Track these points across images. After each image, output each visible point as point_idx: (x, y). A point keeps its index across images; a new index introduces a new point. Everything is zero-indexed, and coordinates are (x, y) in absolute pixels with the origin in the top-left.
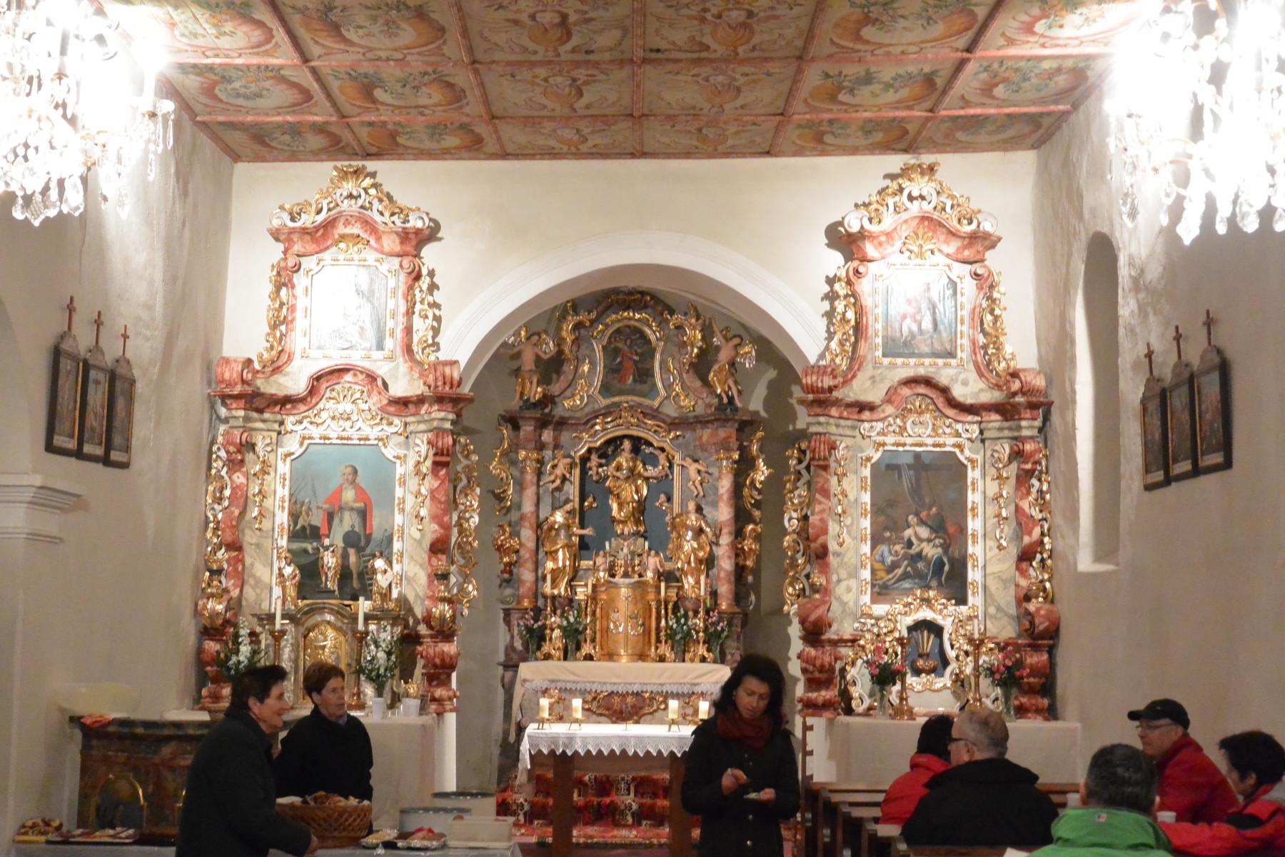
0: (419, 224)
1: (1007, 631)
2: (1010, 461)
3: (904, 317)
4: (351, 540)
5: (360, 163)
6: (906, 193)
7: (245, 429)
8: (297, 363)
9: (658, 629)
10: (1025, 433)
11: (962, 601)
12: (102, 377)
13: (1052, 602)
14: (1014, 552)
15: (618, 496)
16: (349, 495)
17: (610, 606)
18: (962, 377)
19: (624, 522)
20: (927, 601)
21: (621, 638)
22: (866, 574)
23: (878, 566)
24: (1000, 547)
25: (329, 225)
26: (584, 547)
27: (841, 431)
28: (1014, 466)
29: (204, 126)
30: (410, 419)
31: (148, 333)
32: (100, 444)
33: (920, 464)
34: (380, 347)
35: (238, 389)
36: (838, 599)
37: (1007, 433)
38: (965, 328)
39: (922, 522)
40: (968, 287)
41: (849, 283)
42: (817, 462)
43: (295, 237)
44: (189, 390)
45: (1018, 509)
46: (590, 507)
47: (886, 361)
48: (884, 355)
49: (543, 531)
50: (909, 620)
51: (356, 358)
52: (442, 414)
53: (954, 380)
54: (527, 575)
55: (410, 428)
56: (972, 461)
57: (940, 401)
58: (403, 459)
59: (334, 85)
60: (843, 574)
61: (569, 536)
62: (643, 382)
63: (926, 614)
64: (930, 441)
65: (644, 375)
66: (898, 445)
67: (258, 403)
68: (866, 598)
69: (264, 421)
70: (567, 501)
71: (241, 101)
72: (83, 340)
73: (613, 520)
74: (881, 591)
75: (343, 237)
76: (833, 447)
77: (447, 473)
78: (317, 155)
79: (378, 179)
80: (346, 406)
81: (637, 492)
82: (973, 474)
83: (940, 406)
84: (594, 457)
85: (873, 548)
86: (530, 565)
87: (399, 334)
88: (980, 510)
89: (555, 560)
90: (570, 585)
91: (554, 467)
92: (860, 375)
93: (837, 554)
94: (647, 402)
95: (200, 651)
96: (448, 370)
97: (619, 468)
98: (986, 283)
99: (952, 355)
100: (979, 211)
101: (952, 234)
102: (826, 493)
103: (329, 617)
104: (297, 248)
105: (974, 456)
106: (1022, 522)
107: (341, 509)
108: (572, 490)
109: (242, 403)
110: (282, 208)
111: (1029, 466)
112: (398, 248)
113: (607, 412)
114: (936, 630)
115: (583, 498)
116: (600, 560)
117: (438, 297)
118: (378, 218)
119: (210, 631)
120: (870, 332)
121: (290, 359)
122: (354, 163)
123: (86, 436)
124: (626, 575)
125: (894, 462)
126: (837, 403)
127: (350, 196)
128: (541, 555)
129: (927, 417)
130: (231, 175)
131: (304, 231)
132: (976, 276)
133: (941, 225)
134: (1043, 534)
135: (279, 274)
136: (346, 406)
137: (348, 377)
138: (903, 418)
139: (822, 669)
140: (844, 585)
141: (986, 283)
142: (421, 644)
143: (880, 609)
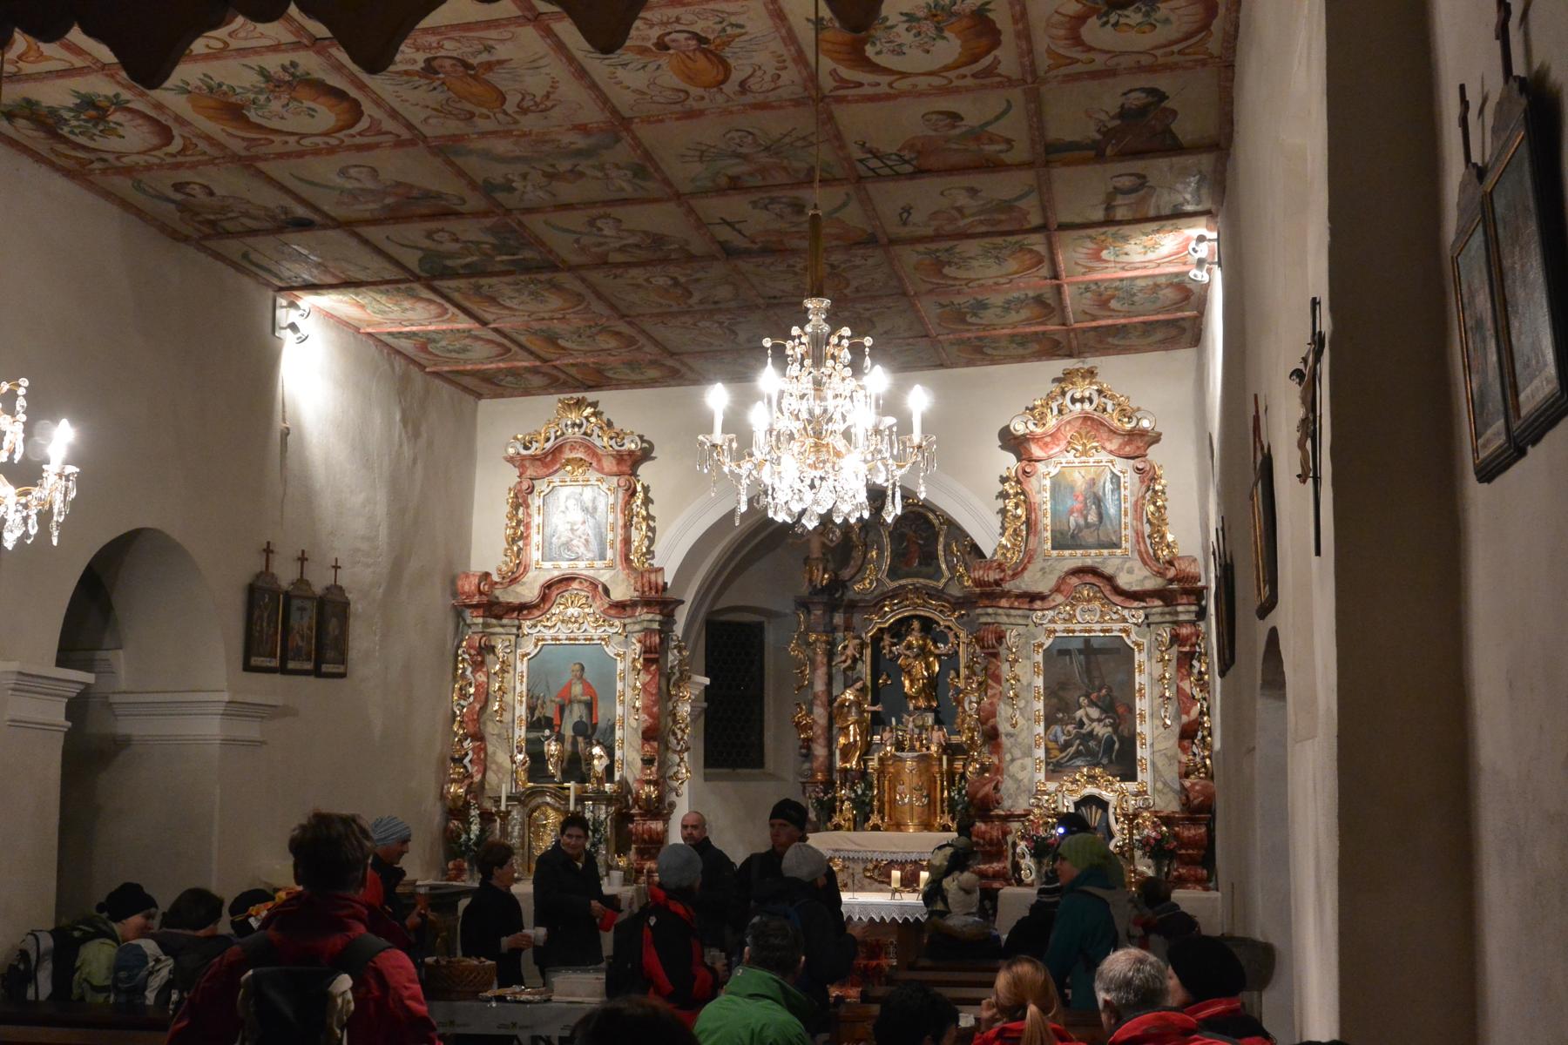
0: (633, 446)
1: (1170, 805)
2: (1171, 644)
3: (1071, 512)
4: (579, 729)
5: (580, 395)
6: (1068, 396)
7: (484, 634)
8: (531, 574)
9: (942, 800)
10: (1182, 617)
11: (1132, 777)
12: (312, 608)
13: (1212, 778)
14: (1177, 730)
15: (909, 673)
16: (577, 689)
17: (896, 779)
18: (1127, 565)
19: (916, 698)
20: (1092, 779)
21: (907, 808)
22: (1040, 753)
23: (1052, 745)
24: (1165, 726)
25: (557, 450)
26: (878, 722)
27: (1012, 620)
28: (1175, 648)
29: (437, 374)
30: (628, 621)
31: (370, 561)
32: (309, 660)
33: (1089, 649)
34: (602, 557)
35: (476, 600)
36: (1012, 777)
37: (1168, 618)
38: (1128, 519)
39: (1092, 704)
40: (1130, 480)
41: (1018, 482)
42: (991, 646)
43: (527, 463)
44: (436, 600)
45: (1179, 690)
46: (885, 684)
47: (1055, 553)
48: (1054, 548)
49: (835, 712)
50: (1077, 797)
51: (581, 567)
52: (650, 616)
53: (1120, 569)
54: (820, 751)
55: (629, 628)
56: (1138, 645)
57: (1107, 590)
58: (623, 656)
59: (522, 339)
60: (1017, 753)
61: (861, 712)
62: (929, 565)
63: (1090, 790)
64: (1097, 627)
65: (929, 558)
66: (1068, 631)
67: (496, 610)
68: (1041, 776)
69: (503, 626)
70: (859, 679)
71: (454, 355)
72: (286, 574)
73: (906, 696)
74: (1055, 769)
75: (569, 462)
76: (1000, 638)
77: (658, 669)
78: (545, 390)
79: (600, 408)
80: (573, 611)
81: (927, 669)
82: (1139, 657)
83: (1107, 593)
84: (887, 638)
85: (1047, 728)
86: (822, 741)
87: (618, 545)
88: (1147, 691)
89: (847, 735)
90: (864, 758)
91: (845, 648)
92: (1030, 567)
93: (1009, 735)
94: (932, 583)
95: (446, 829)
96: (653, 577)
97: (909, 647)
98: (1148, 477)
99: (1117, 546)
100: (1139, 409)
101: (1113, 432)
102: (997, 679)
103: (548, 799)
104: (530, 472)
105: (1140, 640)
106: (1184, 701)
107: (571, 702)
108: (865, 669)
109: (481, 612)
110: (516, 438)
111: (1187, 649)
112: (615, 469)
113: (894, 594)
114: (1103, 805)
115: (875, 675)
116: (886, 735)
117: (653, 510)
118: (598, 442)
119: (457, 811)
120: (1040, 527)
121: (526, 570)
122: (575, 395)
123: (291, 654)
124: (912, 749)
125: (1064, 647)
126: (1006, 594)
127: (574, 425)
128: (835, 731)
129: (1096, 605)
130: (475, 411)
131: (534, 458)
132: (1138, 470)
133: (1102, 424)
134: (1202, 713)
135: (516, 496)
136: (573, 611)
137: (575, 585)
138: (1073, 606)
139: (991, 842)
140: (1018, 763)
141: (1148, 477)
142: (632, 821)
143: (1052, 786)
